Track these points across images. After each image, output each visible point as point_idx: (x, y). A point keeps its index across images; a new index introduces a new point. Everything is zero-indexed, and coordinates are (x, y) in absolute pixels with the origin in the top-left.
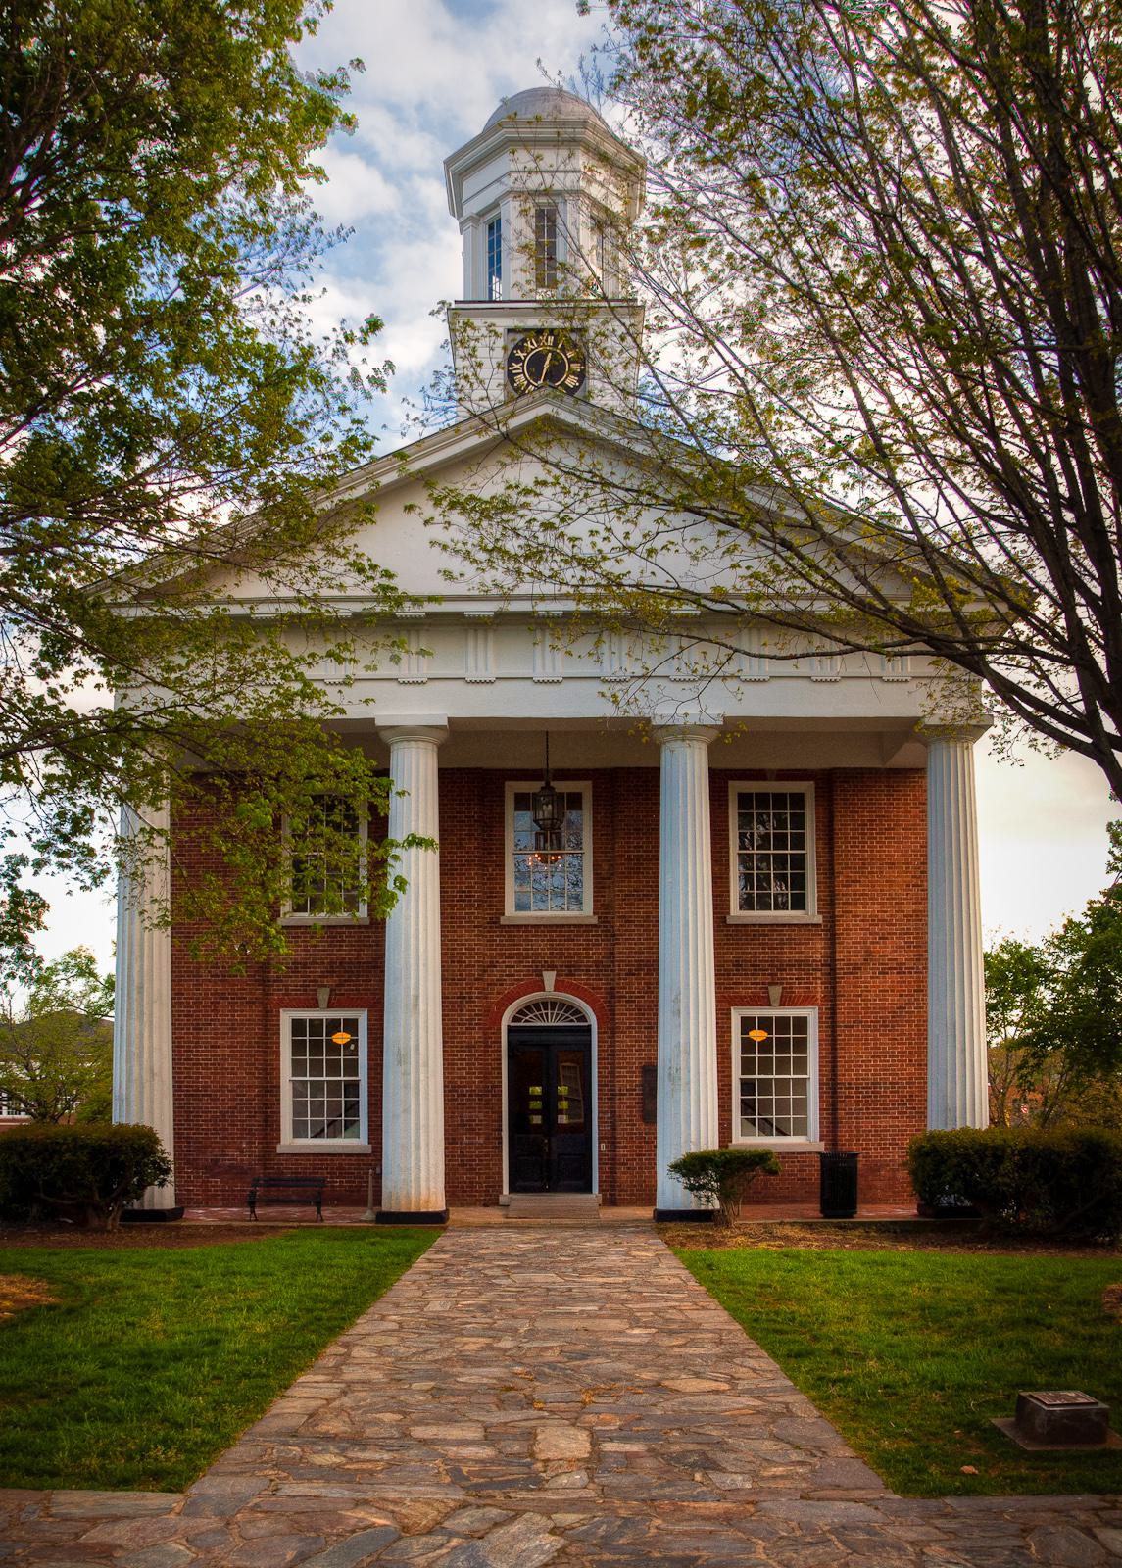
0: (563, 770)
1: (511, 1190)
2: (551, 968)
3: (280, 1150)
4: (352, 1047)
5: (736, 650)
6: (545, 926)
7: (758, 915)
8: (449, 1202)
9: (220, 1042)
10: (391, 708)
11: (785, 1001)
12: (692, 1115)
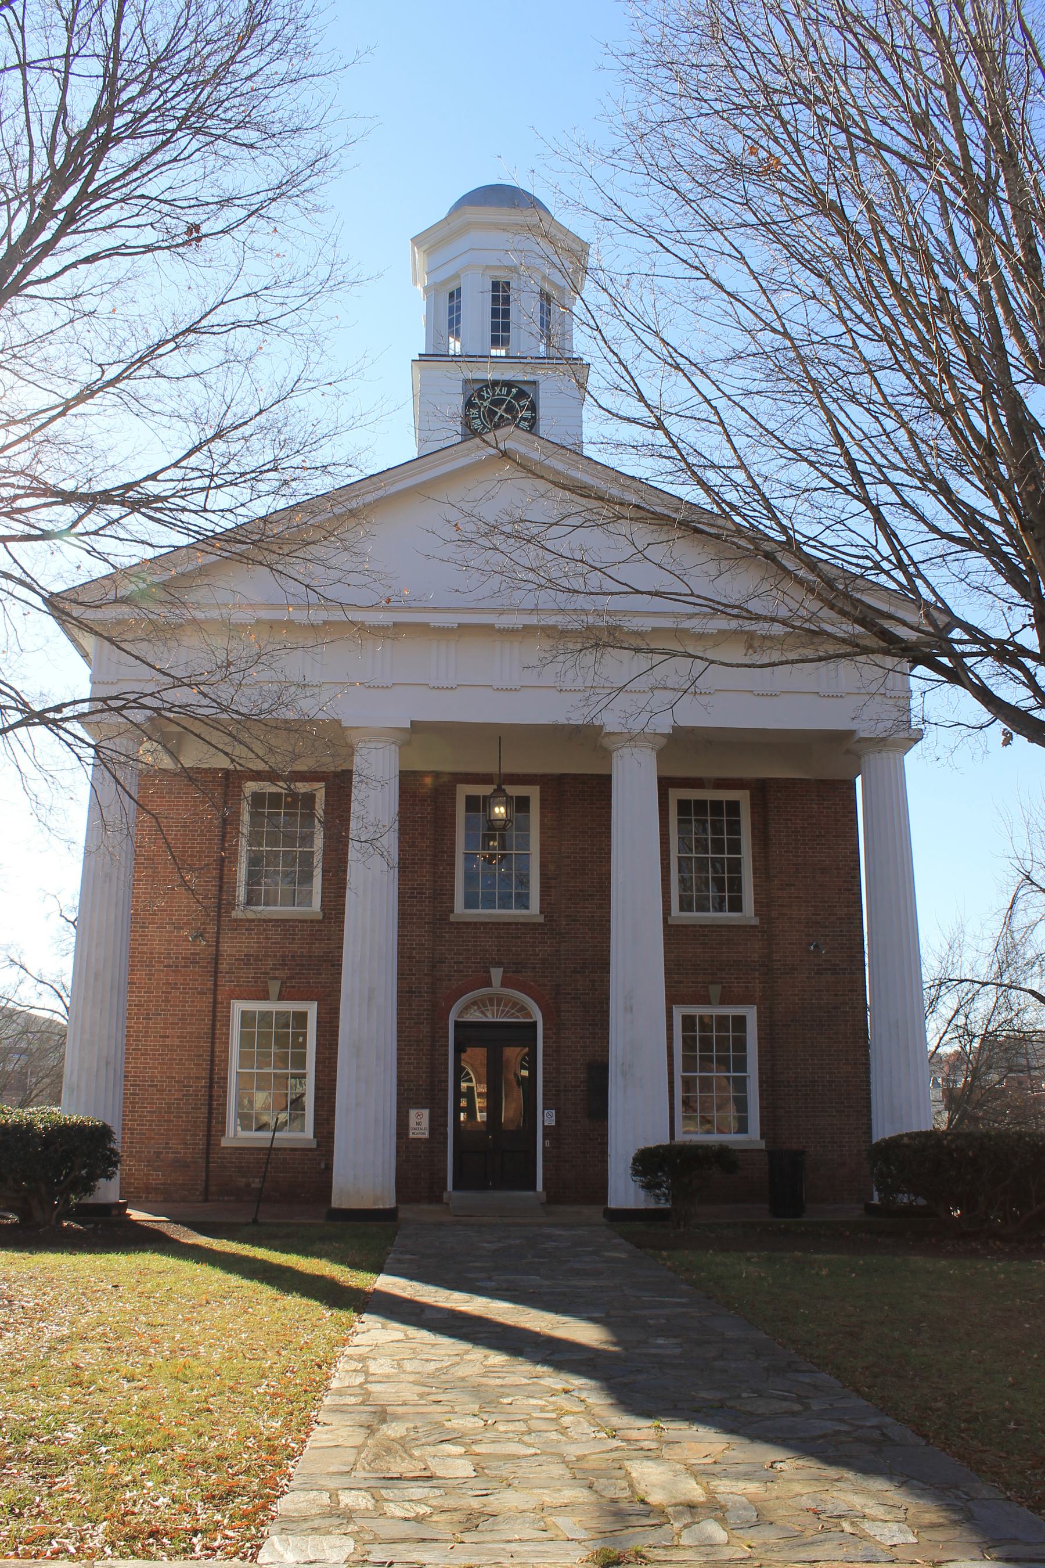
0: (512, 775)
1: (456, 1187)
2: (499, 964)
3: (224, 1143)
4: (301, 1039)
5: (712, 662)
6: (493, 924)
7: (695, 916)
8: (398, 1201)
9: (168, 1032)
10: (354, 710)
11: (724, 1001)
12: (640, 1113)
